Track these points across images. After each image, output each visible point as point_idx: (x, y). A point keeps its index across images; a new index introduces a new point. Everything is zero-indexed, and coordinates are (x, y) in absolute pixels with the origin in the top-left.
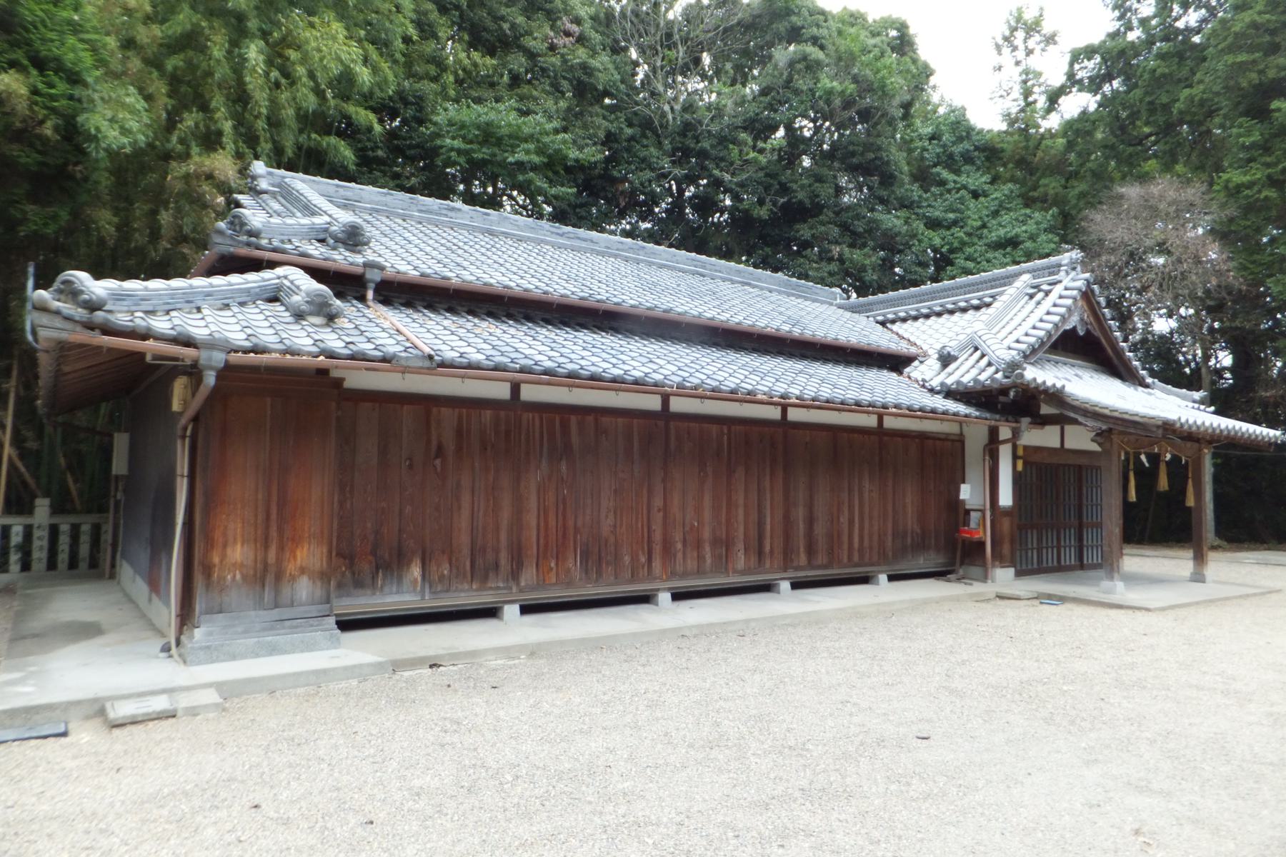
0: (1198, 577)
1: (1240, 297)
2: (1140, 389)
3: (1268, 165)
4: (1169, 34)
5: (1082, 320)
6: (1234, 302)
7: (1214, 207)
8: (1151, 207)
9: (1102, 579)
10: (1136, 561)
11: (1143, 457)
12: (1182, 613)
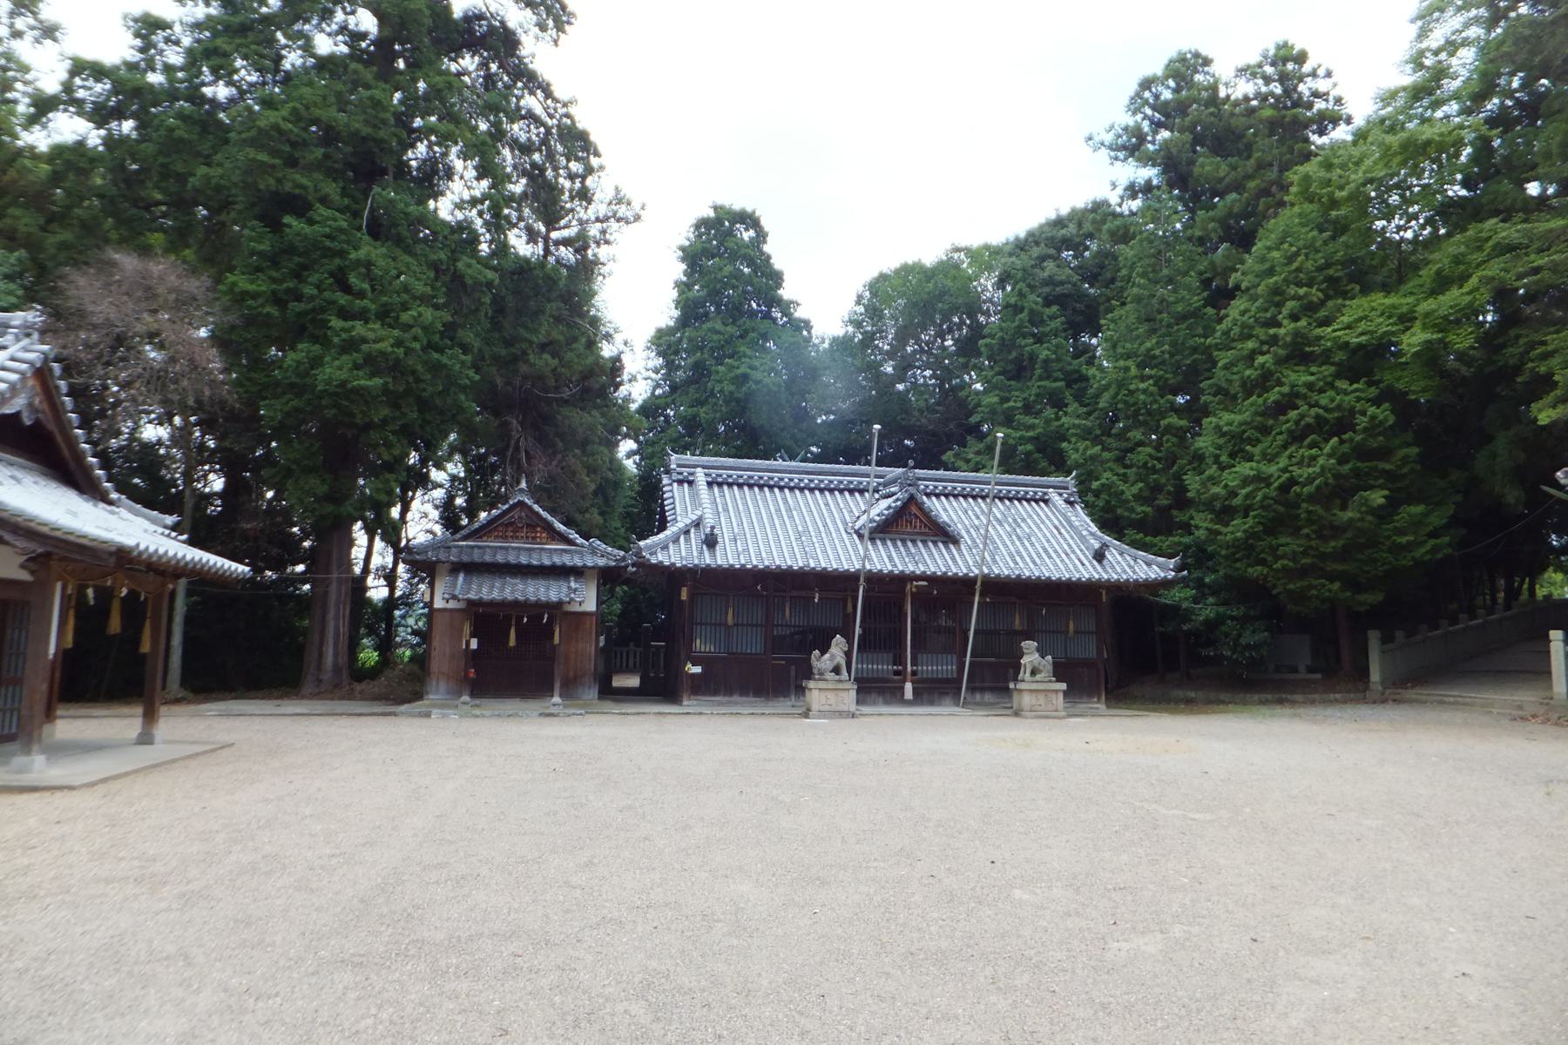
0: (145, 739)
1: (233, 416)
2: (102, 505)
3: (274, 280)
4: (196, 97)
5: (30, 405)
6: (226, 419)
7: (217, 307)
8: (149, 288)
9: (13, 754)
10: (70, 726)
11: (90, 592)
12: (114, 786)
